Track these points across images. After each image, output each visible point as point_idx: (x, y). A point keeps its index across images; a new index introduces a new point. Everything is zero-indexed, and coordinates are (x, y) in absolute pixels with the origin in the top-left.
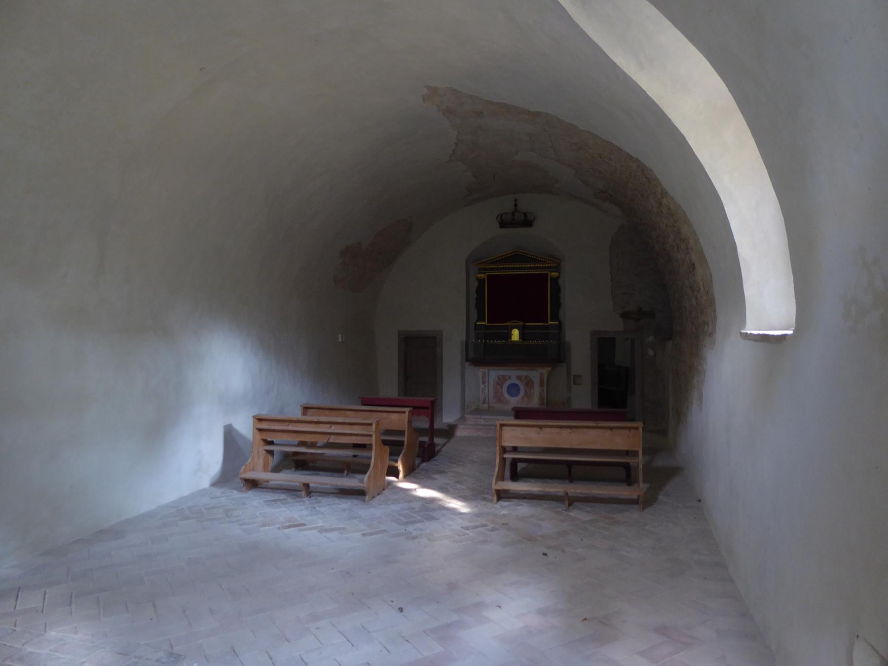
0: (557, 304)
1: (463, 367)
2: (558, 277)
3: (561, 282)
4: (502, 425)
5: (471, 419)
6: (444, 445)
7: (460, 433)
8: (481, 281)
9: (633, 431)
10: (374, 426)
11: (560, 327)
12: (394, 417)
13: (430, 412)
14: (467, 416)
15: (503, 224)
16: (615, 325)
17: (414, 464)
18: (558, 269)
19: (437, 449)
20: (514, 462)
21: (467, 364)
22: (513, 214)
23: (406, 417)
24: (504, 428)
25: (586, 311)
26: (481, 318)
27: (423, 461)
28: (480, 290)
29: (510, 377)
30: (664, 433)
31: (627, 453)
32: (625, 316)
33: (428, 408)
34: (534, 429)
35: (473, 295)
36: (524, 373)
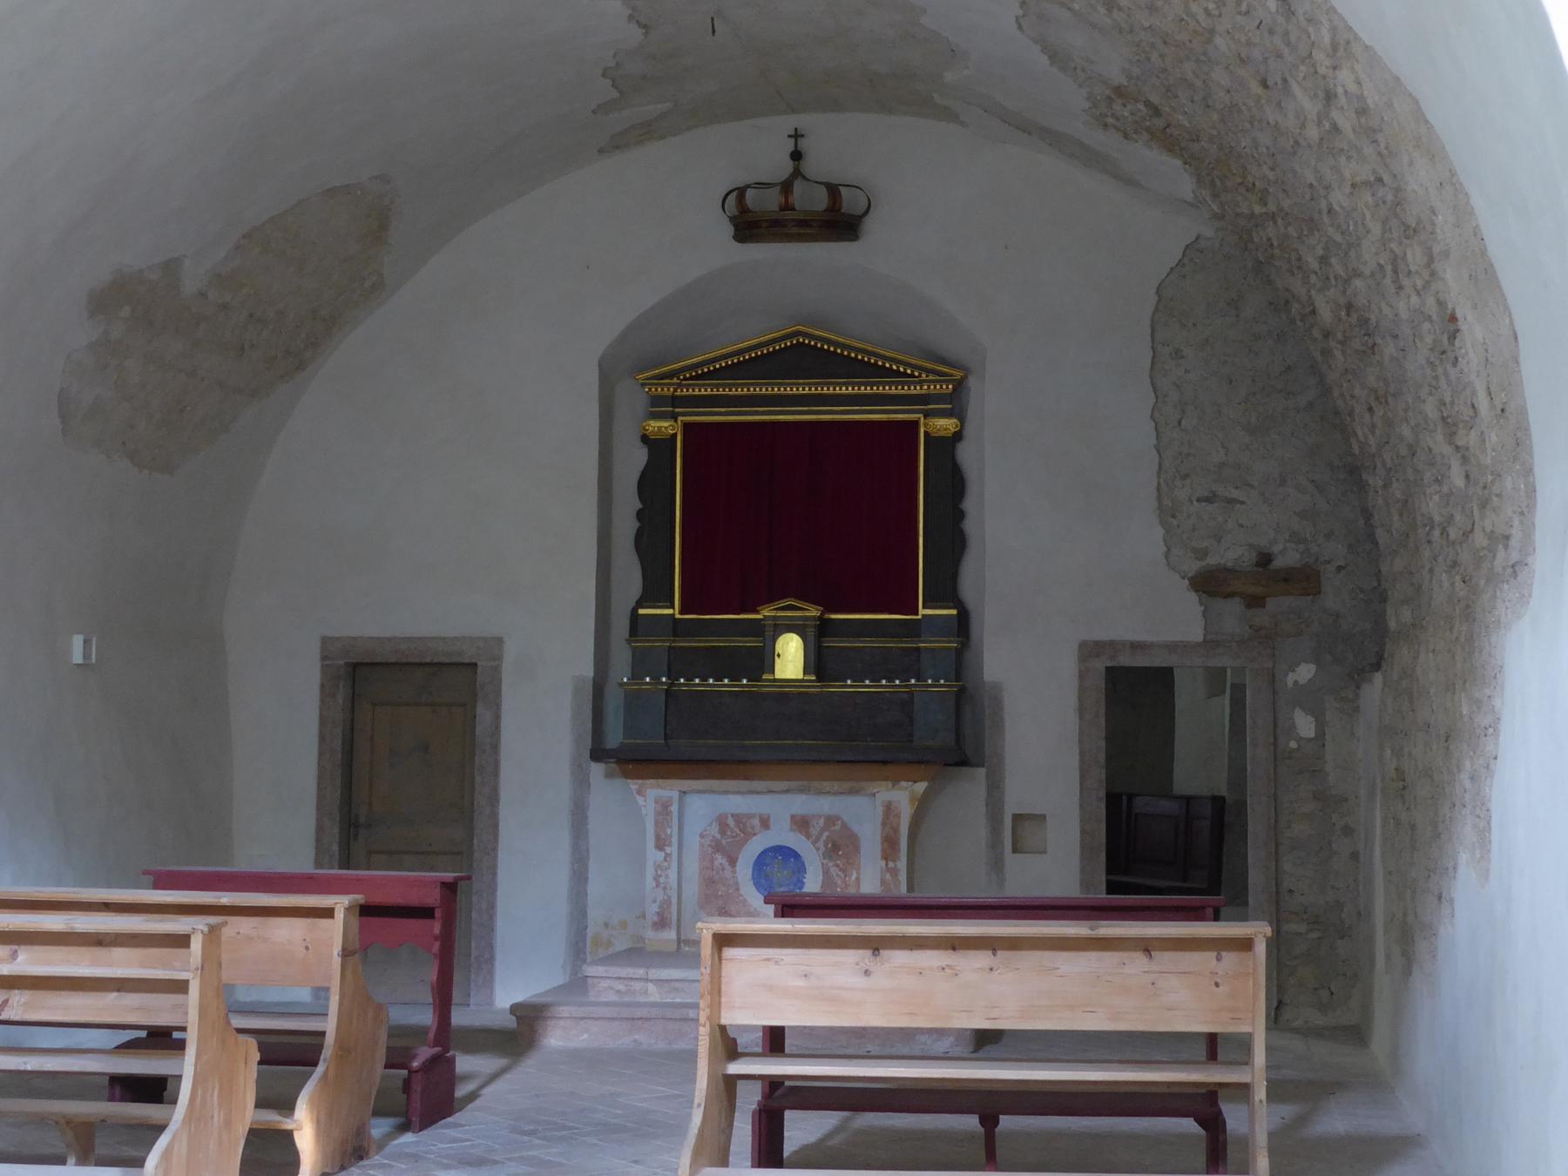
0: (951, 541)
1: (581, 783)
2: (958, 436)
3: (966, 454)
4: (724, 941)
5: (608, 982)
6: (494, 1077)
7: (556, 1038)
8: (658, 448)
9: (1230, 958)
10: (196, 944)
11: (963, 625)
12: (287, 932)
13: (437, 927)
14: (591, 970)
15: (749, 226)
16: (1167, 620)
17: (361, 1131)
18: (955, 403)
19: (461, 1091)
20: (780, 1098)
21: (597, 770)
22: (786, 187)
23: (334, 932)
24: (729, 952)
25: (1061, 564)
26: (655, 591)
27: (404, 1128)
28: (652, 484)
29: (765, 823)
30: (1357, 1034)
31: (1212, 1046)
32: (1209, 584)
33: (425, 913)
34: (849, 956)
35: (627, 503)
36: (820, 804)
